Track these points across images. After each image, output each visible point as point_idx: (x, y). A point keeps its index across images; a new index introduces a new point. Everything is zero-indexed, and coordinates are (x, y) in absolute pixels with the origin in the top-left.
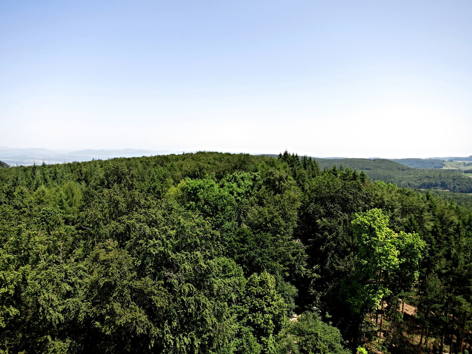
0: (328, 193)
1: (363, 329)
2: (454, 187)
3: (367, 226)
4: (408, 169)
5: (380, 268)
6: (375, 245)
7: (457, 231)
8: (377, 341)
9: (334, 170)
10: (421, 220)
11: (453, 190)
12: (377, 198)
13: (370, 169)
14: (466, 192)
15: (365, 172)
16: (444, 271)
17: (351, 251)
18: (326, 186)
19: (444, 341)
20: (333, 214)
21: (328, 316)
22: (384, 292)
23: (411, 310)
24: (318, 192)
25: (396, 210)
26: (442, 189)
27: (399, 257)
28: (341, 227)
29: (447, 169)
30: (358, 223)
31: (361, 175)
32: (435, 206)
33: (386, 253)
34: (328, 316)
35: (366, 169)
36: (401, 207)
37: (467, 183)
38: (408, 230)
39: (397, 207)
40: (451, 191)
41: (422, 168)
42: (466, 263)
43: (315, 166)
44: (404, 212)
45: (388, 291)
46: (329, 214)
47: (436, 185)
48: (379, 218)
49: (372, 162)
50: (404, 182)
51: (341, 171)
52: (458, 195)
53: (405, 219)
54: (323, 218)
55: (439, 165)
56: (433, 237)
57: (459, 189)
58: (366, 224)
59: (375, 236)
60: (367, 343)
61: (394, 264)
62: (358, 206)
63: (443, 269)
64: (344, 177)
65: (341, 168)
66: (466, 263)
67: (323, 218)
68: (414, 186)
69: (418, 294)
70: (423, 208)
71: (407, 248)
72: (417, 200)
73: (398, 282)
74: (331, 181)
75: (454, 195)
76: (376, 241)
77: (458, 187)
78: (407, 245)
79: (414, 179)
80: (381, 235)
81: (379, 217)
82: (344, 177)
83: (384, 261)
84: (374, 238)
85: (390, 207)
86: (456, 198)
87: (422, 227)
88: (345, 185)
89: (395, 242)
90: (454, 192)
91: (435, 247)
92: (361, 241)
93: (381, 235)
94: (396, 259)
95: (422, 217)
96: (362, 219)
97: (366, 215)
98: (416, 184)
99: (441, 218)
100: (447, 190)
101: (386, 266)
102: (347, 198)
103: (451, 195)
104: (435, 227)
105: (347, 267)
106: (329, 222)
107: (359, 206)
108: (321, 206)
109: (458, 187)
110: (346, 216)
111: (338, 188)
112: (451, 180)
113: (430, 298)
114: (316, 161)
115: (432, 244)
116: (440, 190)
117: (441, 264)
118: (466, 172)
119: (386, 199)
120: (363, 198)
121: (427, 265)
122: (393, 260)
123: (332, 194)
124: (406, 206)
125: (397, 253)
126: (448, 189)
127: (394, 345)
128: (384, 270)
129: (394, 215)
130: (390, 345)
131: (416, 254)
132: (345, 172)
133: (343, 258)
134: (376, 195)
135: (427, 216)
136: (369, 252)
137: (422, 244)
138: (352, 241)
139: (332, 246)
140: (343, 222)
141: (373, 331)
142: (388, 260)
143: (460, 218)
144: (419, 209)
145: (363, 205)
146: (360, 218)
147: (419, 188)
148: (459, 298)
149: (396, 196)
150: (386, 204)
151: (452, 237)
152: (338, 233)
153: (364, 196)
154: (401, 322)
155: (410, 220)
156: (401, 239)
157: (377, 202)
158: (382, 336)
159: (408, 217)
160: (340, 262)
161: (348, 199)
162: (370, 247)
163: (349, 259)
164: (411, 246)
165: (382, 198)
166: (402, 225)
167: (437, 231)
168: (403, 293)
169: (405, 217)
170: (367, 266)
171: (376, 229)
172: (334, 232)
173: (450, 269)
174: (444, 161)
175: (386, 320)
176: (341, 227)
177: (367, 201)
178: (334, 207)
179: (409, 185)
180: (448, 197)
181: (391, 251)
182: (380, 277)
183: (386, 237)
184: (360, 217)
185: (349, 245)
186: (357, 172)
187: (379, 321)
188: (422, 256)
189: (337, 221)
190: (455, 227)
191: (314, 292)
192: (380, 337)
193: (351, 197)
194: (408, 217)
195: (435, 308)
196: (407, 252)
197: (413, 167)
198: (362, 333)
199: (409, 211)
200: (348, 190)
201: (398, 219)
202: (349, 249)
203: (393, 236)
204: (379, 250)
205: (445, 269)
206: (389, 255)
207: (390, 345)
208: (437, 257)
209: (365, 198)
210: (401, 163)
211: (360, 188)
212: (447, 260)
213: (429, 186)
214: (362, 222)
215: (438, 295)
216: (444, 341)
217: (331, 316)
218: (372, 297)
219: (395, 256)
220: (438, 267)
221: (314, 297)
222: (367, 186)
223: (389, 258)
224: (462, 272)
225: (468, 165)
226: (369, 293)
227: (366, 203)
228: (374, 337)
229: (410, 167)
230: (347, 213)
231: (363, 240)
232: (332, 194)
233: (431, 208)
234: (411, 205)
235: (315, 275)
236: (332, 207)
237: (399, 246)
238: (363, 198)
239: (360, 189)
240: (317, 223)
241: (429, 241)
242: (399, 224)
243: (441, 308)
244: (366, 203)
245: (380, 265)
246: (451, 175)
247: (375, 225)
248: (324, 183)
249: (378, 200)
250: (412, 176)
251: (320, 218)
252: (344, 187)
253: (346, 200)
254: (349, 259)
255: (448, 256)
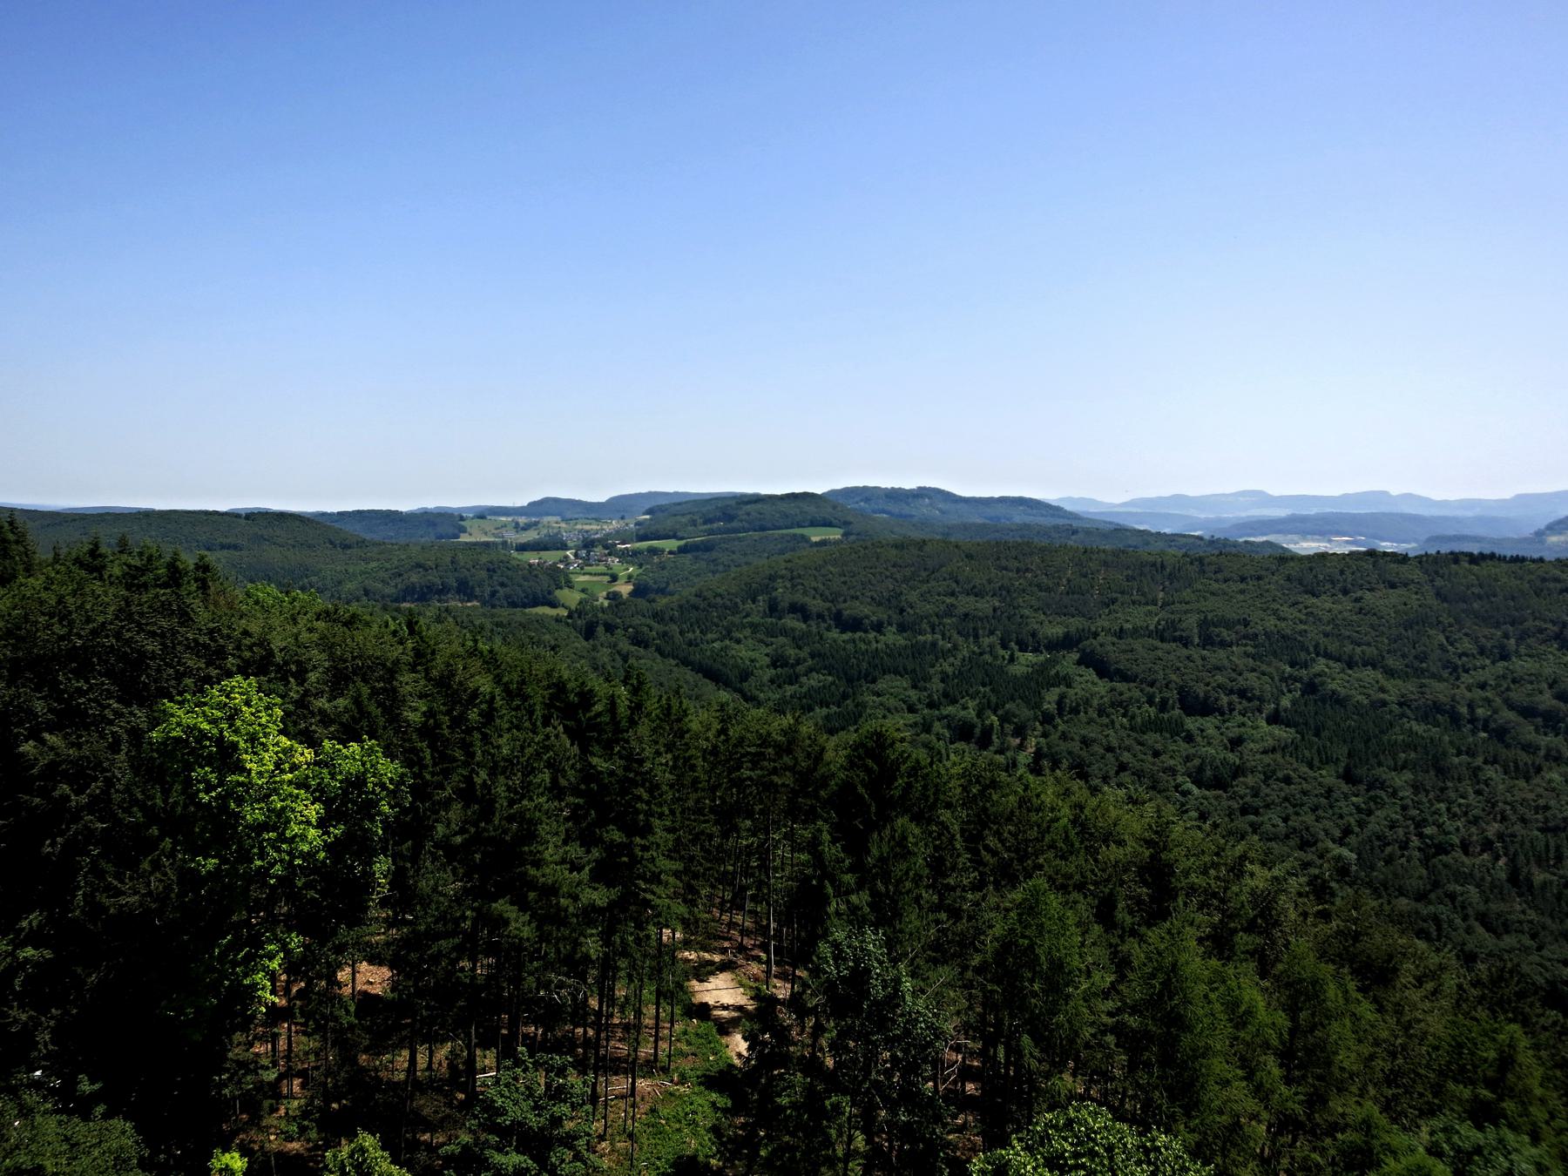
0: (62, 638)
1: (226, 1091)
2: (493, 594)
3: (210, 739)
4: (362, 543)
5: (263, 873)
6: (240, 801)
7: (489, 716)
8: (282, 1112)
9: (94, 552)
10: (392, 701)
11: (490, 601)
12: (247, 641)
13: (236, 547)
14: (525, 606)
15: (211, 557)
16: (459, 839)
17: (161, 838)
18: (52, 616)
19: (474, 1041)
20: (85, 714)
21: (86, 1087)
22: (284, 947)
23: (373, 978)
24: (20, 639)
25: (313, 677)
26: (462, 601)
27: (322, 824)
28: (122, 756)
29: (472, 539)
30: (174, 734)
31: (197, 567)
32: (433, 653)
33: (278, 820)
34: (86, 1087)
35: (223, 547)
36: (327, 664)
37: (525, 578)
38: (348, 734)
39: (315, 667)
40: (484, 604)
41: (403, 541)
42: (512, 803)
43: (17, 542)
44: (339, 680)
45: (295, 941)
46: (70, 718)
47: (443, 591)
48: (250, 705)
49: (243, 522)
50: (349, 586)
51: (124, 557)
52: (504, 613)
53: (341, 702)
54: (47, 736)
55: (451, 531)
56: (425, 744)
57: (507, 597)
58: (204, 735)
59: (240, 768)
60: (245, 1131)
61: (306, 848)
62: (179, 677)
63: (456, 834)
64: (134, 579)
65: (123, 546)
66: (512, 803)
67: (47, 736)
68: (383, 597)
69: (391, 923)
70: (397, 662)
71: (345, 792)
72: (377, 638)
73: (327, 904)
74: (74, 593)
75: (493, 616)
76: (240, 784)
77: (502, 591)
78: (346, 781)
79: (382, 574)
80: (261, 762)
81: (248, 703)
82: (134, 577)
83: (273, 847)
84: (235, 778)
85: (294, 668)
86: (497, 625)
87: (394, 718)
88: (128, 604)
89: (307, 777)
90: (493, 606)
91: (433, 774)
92: (192, 797)
93: (258, 765)
94: (312, 833)
95: (394, 690)
96: (188, 720)
97: (205, 704)
98: (387, 591)
99: (444, 683)
100: (476, 603)
101: (282, 861)
102: (138, 651)
103: (484, 615)
104: (430, 714)
105: (150, 893)
106: (73, 745)
107: (184, 675)
108: (38, 689)
109: (502, 591)
110: (140, 715)
111: (101, 619)
112: (484, 574)
113: (422, 928)
114: (19, 521)
115: (423, 767)
116: (455, 604)
117: (450, 823)
118: (522, 548)
119: (277, 643)
120: (195, 648)
121: (410, 830)
122: (303, 837)
123: (79, 643)
124: (345, 661)
125: (313, 811)
126: (476, 598)
127: (335, 1106)
128: (277, 877)
129: (307, 693)
130: (325, 1110)
131: (374, 804)
132: (136, 562)
133: (134, 865)
134: (246, 633)
135: (408, 682)
136: (219, 826)
137: (389, 769)
138: (165, 801)
139: (91, 832)
140: (125, 736)
141: (260, 1086)
142: (285, 841)
143: (498, 680)
144: (384, 665)
145: (199, 669)
146: (182, 717)
147: (396, 600)
148: (501, 906)
149: (310, 630)
150: (278, 659)
151: (477, 735)
152: (109, 783)
153: (204, 639)
154: (351, 1027)
155: (357, 701)
156: (326, 765)
157: (248, 654)
158: (296, 1089)
159: (340, 690)
160: (122, 882)
161: (143, 655)
162: (224, 808)
163: (157, 866)
164: (357, 782)
165: (263, 643)
166: (332, 722)
167: (438, 725)
168: (344, 934)
169: (342, 695)
170: (215, 875)
171: (242, 745)
172: (96, 779)
173: (473, 830)
174: (462, 519)
175: (305, 1033)
176: (122, 756)
177: (215, 656)
178: (91, 689)
179: (366, 592)
180: (477, 623)
181: (293, 810)
182: (272, 900)
183: (278, 765)
184: (180, 713)
185: (151, 815)
186: (183, 556)
187: (282, 1044)
188: (391, 807)
189: (102, 736)
190: (484, 706)
191: (24, 1017)
192: (291, 1096)
193: (152, 646)
194: (340, 690)
195: (440, 951)
196: (346, 803)
197: (377, 537)
198: (228, 1103)
199: (354, 673)
200: (139, 624)
201: (322, 703)
202: (155, 831)
203: (298, 759)
204: (253, 814)
205: (462, 831)
206: (288, 821)
207: (325, 1110)
208: (439, 802)
209: (206, 646)
210: (337, 525)
211: (187, 614)
212: (466, 806)
213: (423, 594)
214: (190, 729)
215: (445, 912)
216: (474, 1041)
217: (96, 1087)
218: (246, 975)
219: (308, 823)
220: (440, 829)
221: (28, 1033)
222: (216, 604)
223: (288, 834)
224: (505, 832)
225: (526, 528)
226: (235, 964)
227: (208, 664)
228: (266, 1103)
229: (368, 537)
230: (141, 705)
231: (199, 791)
232: (79, 643)
233: (422, 657)
234: (360, 657)
235: (29, 952)
236: (79, 690)
237: (320, 788)
238: (195, 648)
239: (185, 617)
240: (23, 755)
241: (411, 759)
242: (326, 719)
243: (454, 948)
244: (208, 664)
245: (259, 863)
246: (484, 559)
247: (236, 732)
248: (42, 602)
249: (250, 648)
250: (374, 564)
251: (34, 734)
252: (124, 613)
253: (140, 660)
254: (157, 866)
255: (467, 794)
